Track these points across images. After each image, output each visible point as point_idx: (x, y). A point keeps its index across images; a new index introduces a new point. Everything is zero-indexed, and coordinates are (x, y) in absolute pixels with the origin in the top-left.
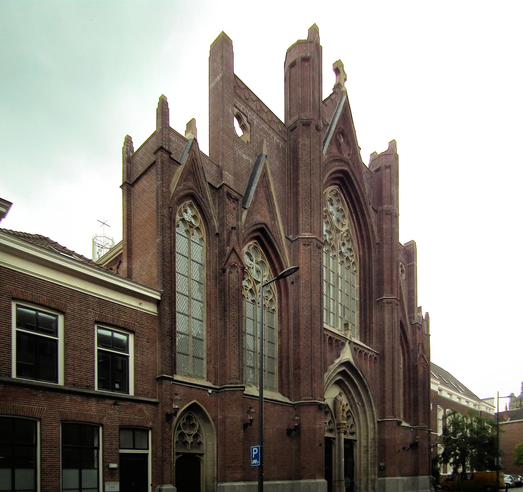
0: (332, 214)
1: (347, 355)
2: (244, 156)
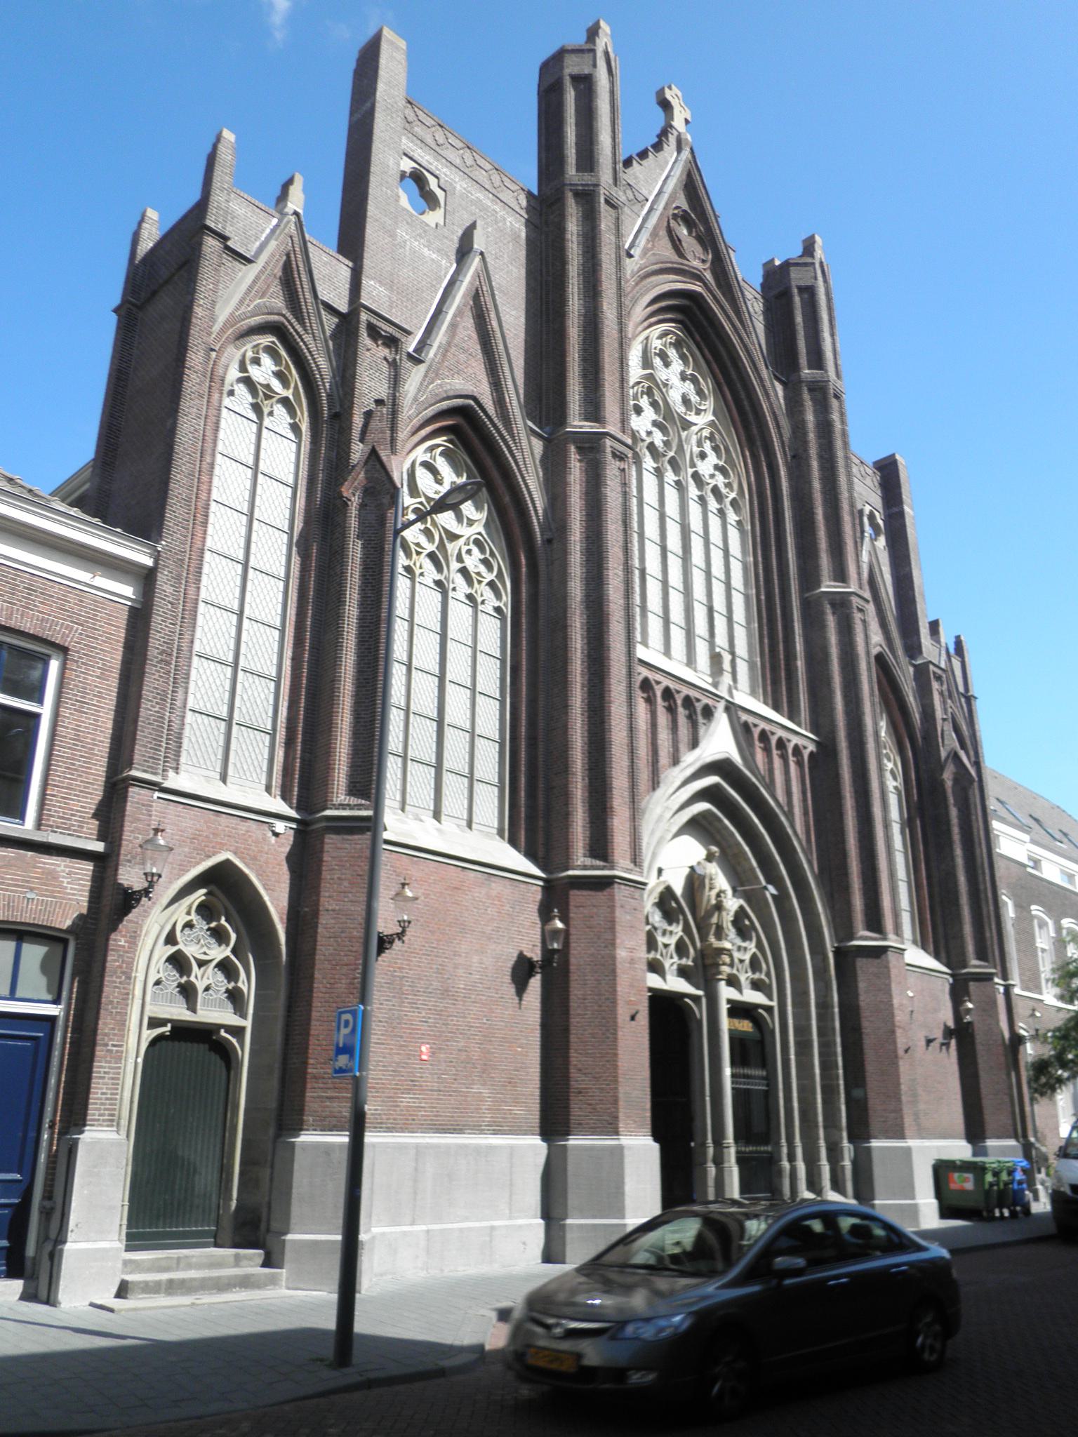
1: (719, 741)
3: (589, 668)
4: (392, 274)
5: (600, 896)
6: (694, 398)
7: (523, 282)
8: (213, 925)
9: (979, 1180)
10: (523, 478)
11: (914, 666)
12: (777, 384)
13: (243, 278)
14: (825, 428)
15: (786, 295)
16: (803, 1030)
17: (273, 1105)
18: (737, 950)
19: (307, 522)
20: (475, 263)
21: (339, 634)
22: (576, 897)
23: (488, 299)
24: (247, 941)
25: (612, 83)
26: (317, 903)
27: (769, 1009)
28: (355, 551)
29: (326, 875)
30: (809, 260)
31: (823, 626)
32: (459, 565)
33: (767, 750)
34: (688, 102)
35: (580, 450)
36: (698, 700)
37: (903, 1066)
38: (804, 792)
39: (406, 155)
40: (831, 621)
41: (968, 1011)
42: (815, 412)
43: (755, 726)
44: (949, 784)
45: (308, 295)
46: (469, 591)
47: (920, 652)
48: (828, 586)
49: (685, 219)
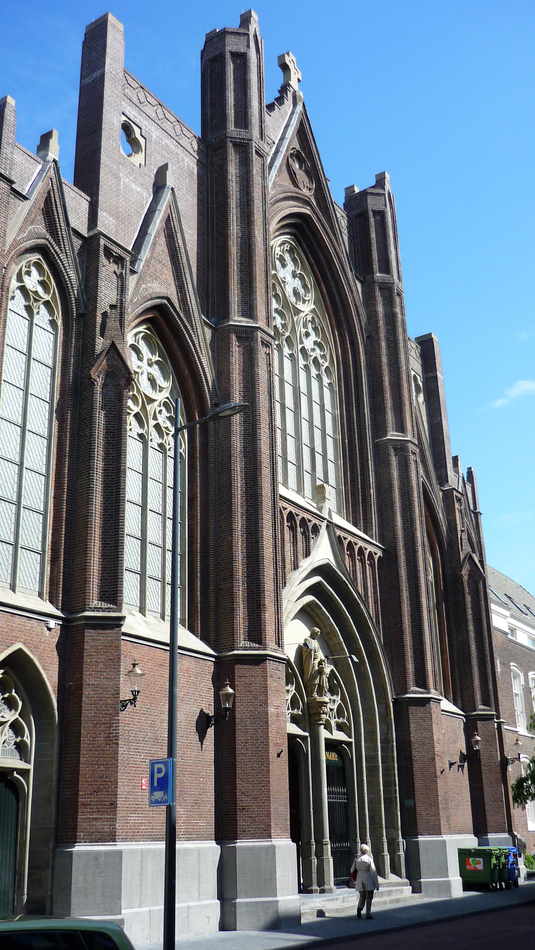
0: (284, 282)
1: (322, 552)
2: (134, 186)
3: (247, 501)
4: (117, 208)
5: (256, 670)
6: (302, 291)
7: (196, 208)
8: (6, 695)
9: (487, 863)
10: (199, 358)
11: (443, 491)
12: (357, 282)
13: (21, 211)
14: (391, 318)
15: (364, 215)
16: (372, 759)
17: (53, 826)
18: (331, 702)
19: (62, 395)
20: (166, 197)
21: (89, 481)
22: (240, 670)
23: (176, 223)
24: (29, 708)
25: (259, 60)
26: (81, 679)
27: (349, 744)
28: (100, 418)
29: (86, 659)
30: (381, 191)
31: (388, 465)
32: (154, 422)
33: (352, 556)
34: (300, 66)
35: (239, 338)
36: (310, 521)
37: (440, 782)
38: (375, 587)
39: (123, 113)
40: (394, 461)
41: (477, 742)
42: (384, 305)
43: (345, 539)
44: (466, 578)
45: (63, 224)
46: (160, 441)
47: (447, 481)
48: (392, 435)
49: (297, 156)
